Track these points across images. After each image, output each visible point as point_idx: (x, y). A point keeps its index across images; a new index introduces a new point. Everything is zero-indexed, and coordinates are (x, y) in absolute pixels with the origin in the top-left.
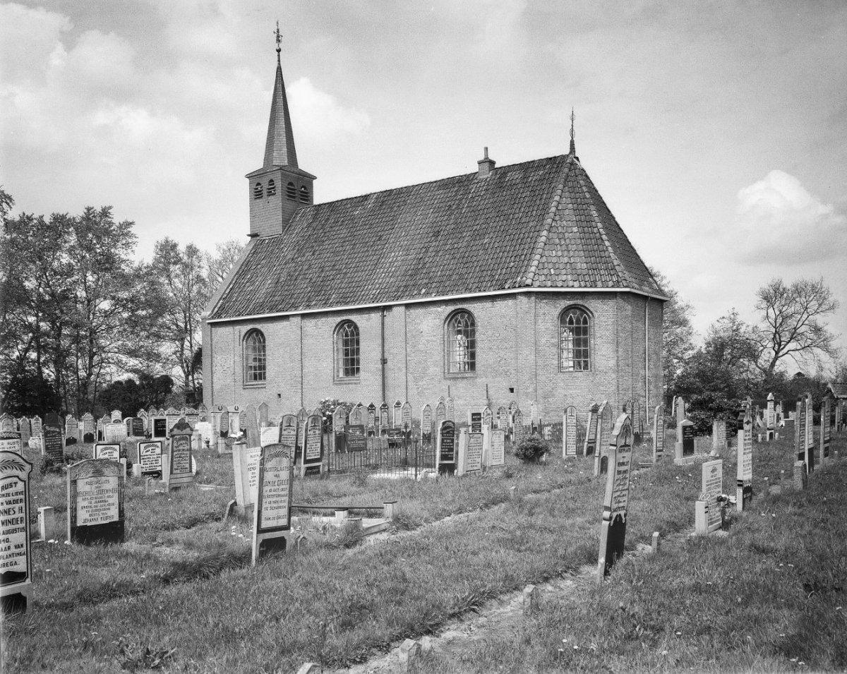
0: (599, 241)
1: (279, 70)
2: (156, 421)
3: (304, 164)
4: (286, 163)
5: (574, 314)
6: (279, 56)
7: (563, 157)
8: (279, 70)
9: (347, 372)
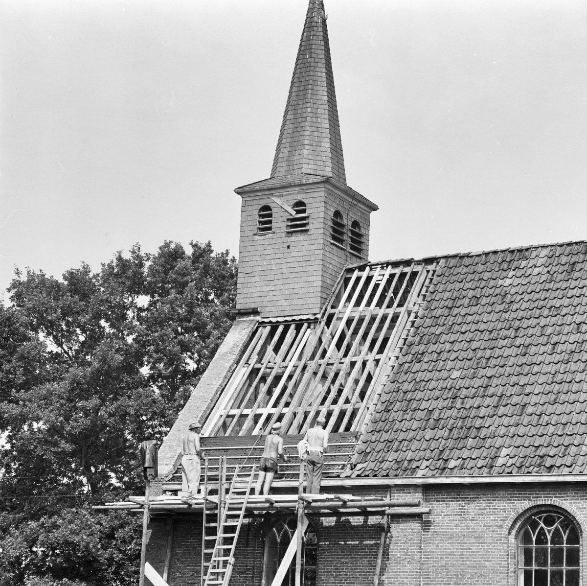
3: (355, 181)
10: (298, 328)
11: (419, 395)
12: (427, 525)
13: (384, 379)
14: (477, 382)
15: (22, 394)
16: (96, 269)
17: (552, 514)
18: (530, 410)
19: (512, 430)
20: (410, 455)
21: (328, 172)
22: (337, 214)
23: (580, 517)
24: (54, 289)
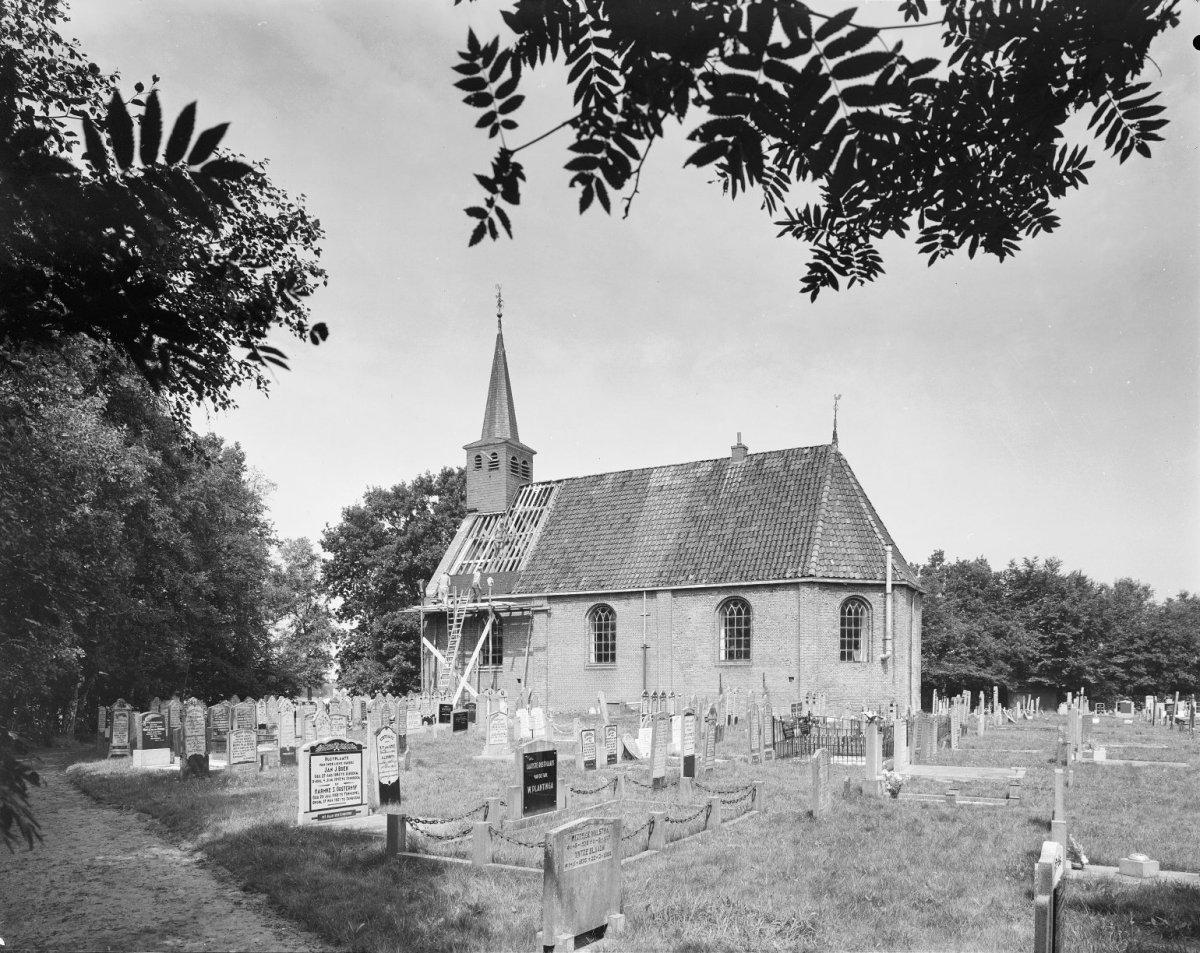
0: (872, 534)
1: (500, 337)
2: (442, 706)
3: (525, 440)
4: (509, 436)
5: (853, 605)
6: (500, 321)
7: (827, 448)
8: (500, 337)
9: (599, 658)
10: (496, 518)
11: (549, 551)
12: (549, 615)
13: (534, 544)
14: (576, 544)
15: (372, 552)
16: (409, 484)
17: (737, 601)
18: (597, 558)
19: (589, 568)
20: (543, 582)
21: (509, 436)
22: (514, 458)
23: (615, 608)
24: (386, 496)
